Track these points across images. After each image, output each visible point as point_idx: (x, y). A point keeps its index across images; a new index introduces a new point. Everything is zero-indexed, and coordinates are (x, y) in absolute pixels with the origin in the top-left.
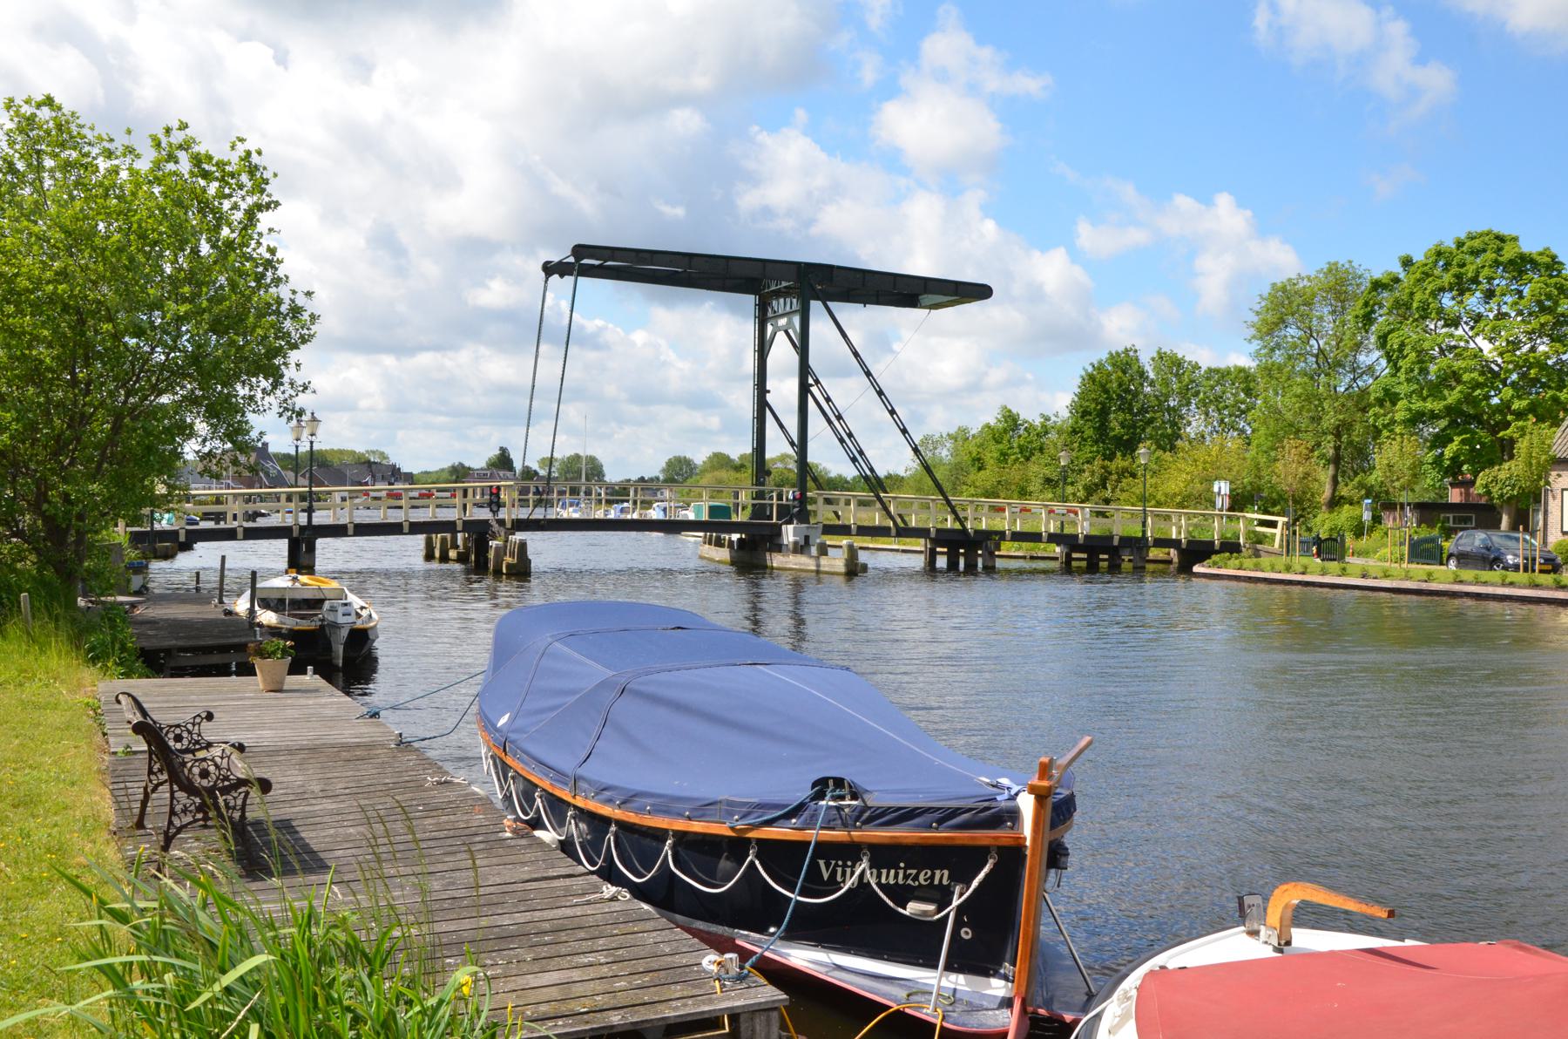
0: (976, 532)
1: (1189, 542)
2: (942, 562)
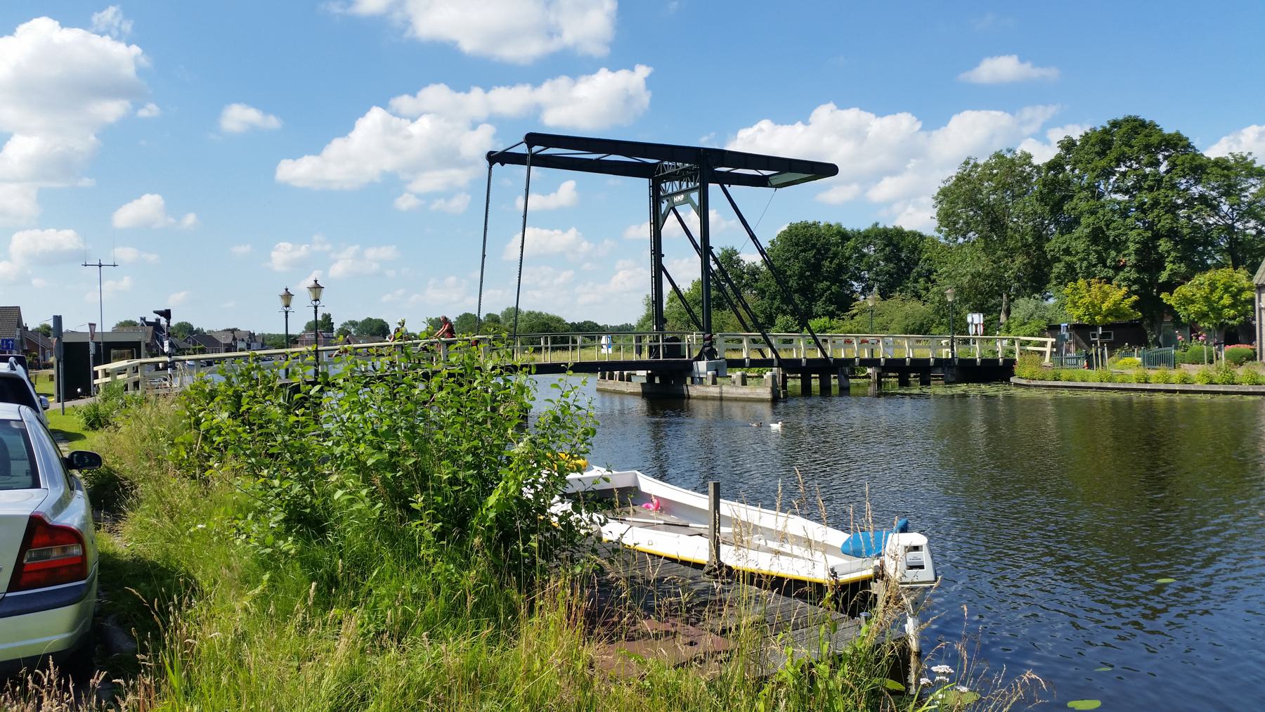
0: (835, 360)
1: (983, 361)
2: (815, 383)
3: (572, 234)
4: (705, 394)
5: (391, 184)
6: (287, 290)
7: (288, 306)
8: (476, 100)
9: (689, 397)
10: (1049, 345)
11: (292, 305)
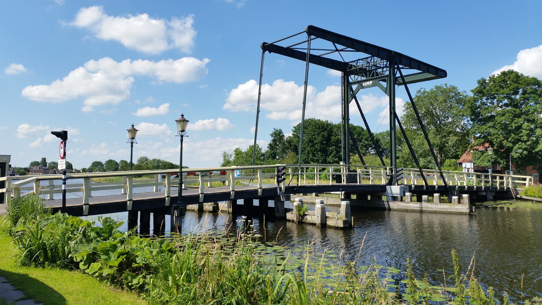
3: (164, 126)
4: (405, 208)
5: (80, 100)
6: (133, 126)
7: (183, 131)
8: (126, 66)
9: (390, 209)
10: (528, 180)
11: (136, 138)
